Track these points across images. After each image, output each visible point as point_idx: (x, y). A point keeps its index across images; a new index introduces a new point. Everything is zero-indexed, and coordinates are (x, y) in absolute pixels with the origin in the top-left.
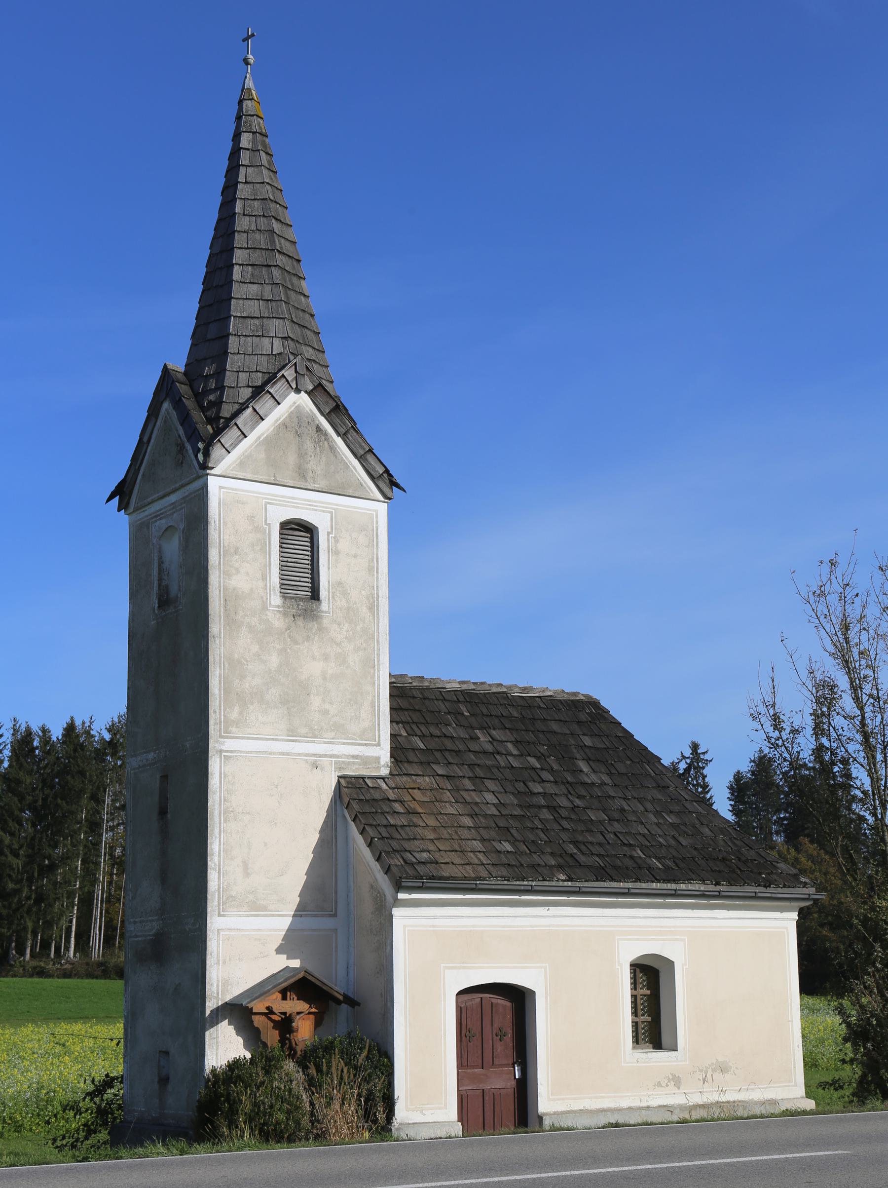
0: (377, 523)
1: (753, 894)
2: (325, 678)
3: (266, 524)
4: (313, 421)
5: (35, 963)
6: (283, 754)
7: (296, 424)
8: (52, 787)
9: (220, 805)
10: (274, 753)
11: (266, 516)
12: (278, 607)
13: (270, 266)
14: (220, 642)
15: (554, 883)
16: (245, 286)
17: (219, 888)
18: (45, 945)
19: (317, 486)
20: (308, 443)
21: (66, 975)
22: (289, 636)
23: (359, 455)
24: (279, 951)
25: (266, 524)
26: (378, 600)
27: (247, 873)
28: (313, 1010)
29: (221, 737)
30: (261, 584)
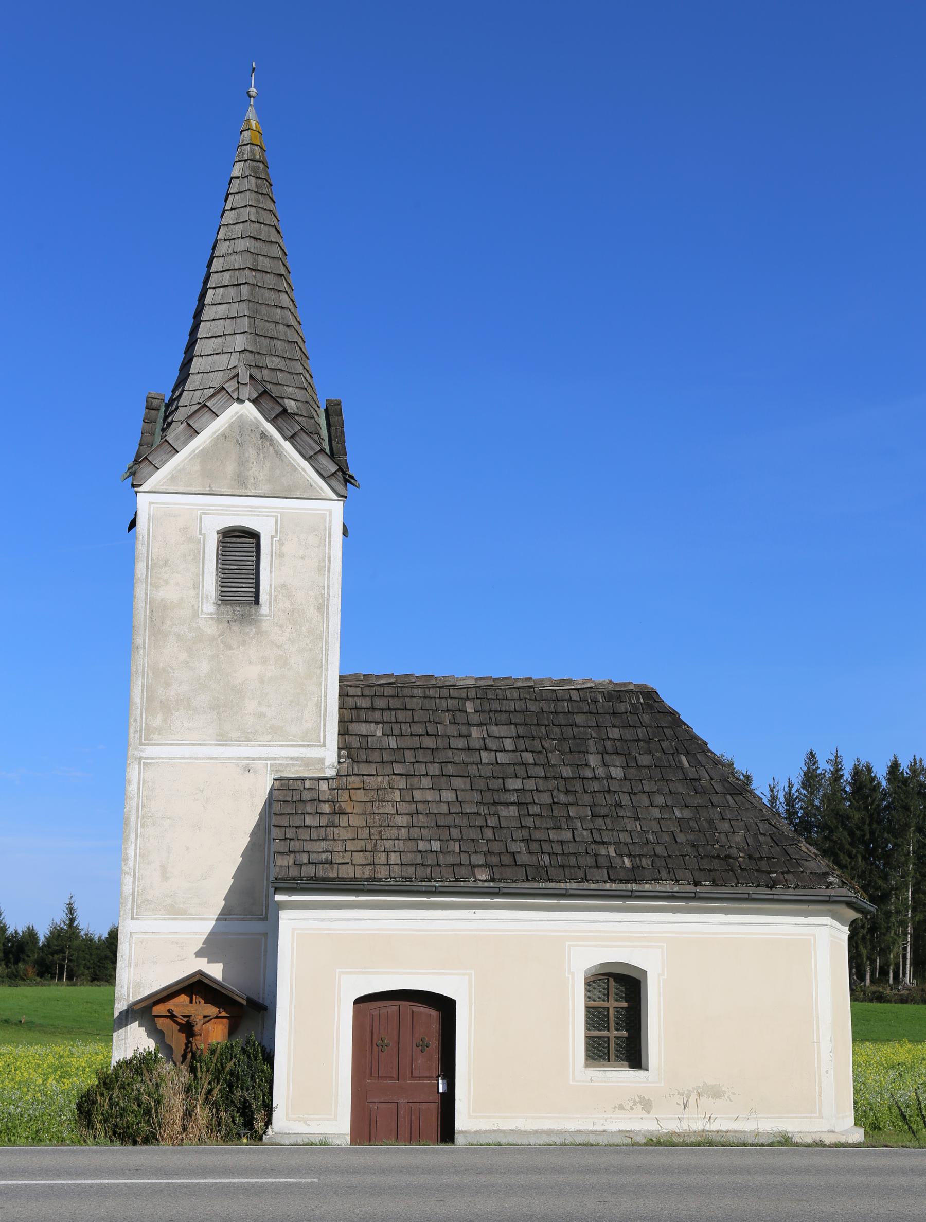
0: (330, 522)
1: (747, 896)
2: (262, 681)
3: (200, 533)
4: (257, 428)
5: (874, 988)
6: (211, 758)
7: (239, 433)
8: (879, 822)
9: (138, 811)
10: (201, 758)
11: (200, 527)
12: (211, 614)
13: (240, 284)
14: (144, 653)
15: (471, 884)
16: (215, 307)
17: (133, 892)
18: (884, 972)
19: (258, 492)
20: (250, 450)
21: (903, 1000)
22: (223, 642)
23: (307, 456)
24: (199, 954)
25: (200, 533)
26: (328, 599)
27: (165, 876)
28: (224, 1014)
29: (141, 744)
30: (192, 593)
